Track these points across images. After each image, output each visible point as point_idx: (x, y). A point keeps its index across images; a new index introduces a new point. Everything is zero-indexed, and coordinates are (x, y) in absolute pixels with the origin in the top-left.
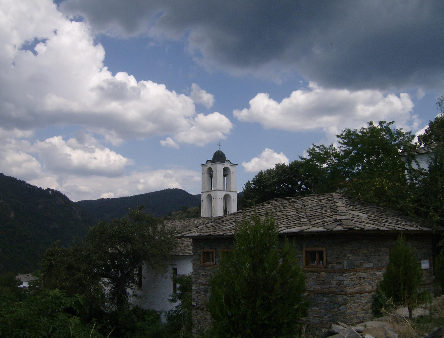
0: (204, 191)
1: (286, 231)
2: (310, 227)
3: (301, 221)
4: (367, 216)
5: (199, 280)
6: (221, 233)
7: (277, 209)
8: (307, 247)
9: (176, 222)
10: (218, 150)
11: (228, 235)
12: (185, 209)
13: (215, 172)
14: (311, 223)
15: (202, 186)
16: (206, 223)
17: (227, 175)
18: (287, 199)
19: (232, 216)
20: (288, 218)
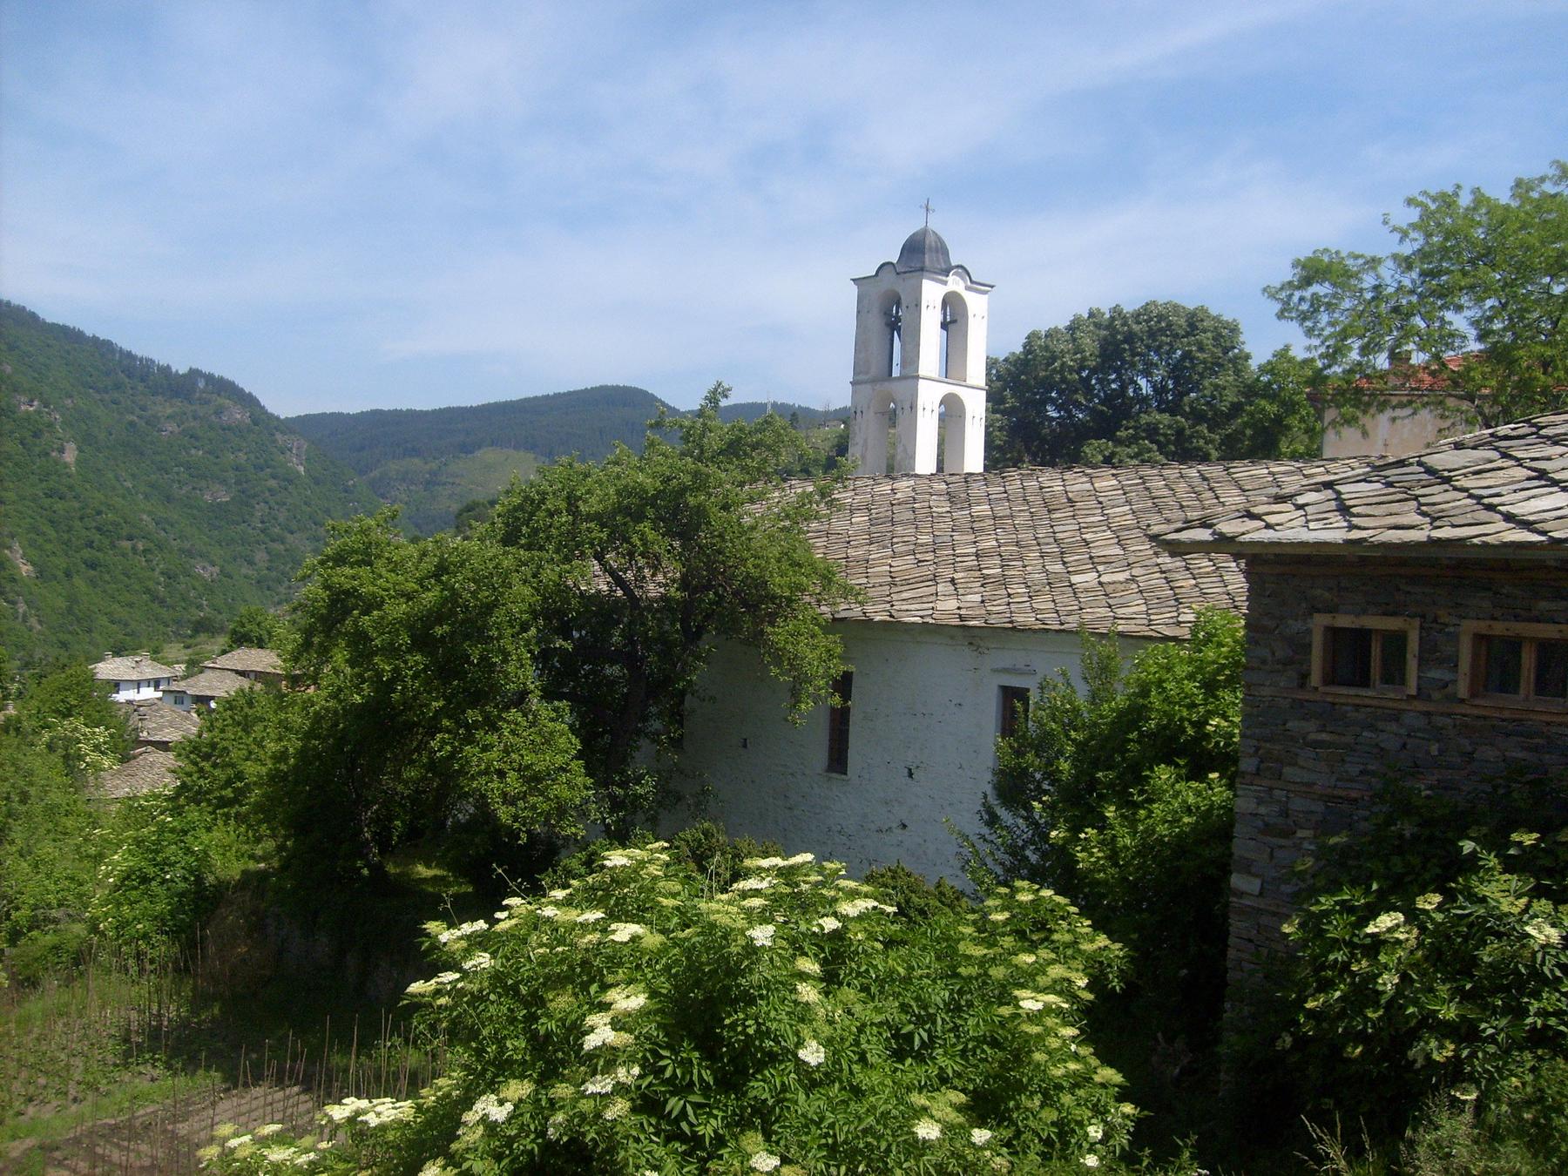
0: (862, 377)
17: (953, 321)
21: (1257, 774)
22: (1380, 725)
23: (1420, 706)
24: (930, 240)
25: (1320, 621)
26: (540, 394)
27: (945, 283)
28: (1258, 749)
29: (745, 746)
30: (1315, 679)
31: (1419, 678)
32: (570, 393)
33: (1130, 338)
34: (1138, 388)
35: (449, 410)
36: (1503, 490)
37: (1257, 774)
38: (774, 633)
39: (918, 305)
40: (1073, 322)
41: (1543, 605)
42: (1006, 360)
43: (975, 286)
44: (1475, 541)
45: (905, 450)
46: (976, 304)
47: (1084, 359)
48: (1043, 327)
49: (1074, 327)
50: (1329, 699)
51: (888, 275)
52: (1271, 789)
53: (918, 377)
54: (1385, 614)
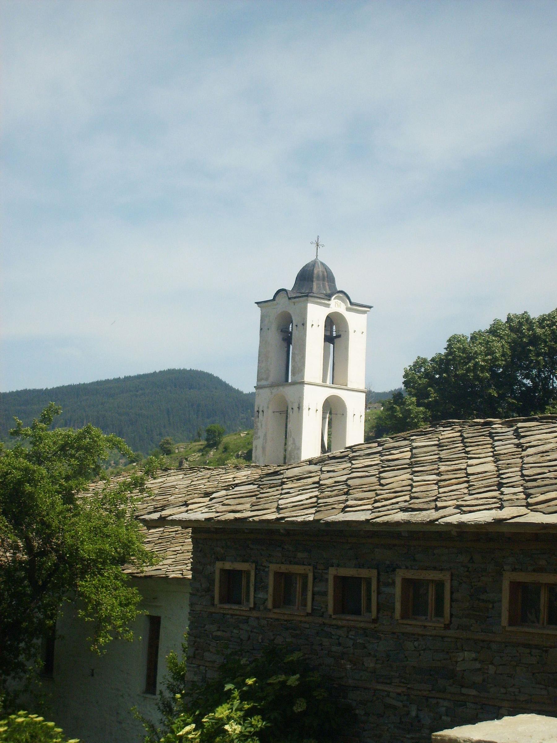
0: (263, 383)
1: (455, 519)
2: (524, 510)
3: (502, 493)
4: (522, 490)
5: (206, 654)
6: (273, 517)
7: (443, 454)
8: (514, 570)
9: (168, 475)
10: (313, 258)
11: (293, 522)
12: (212, 440)
13: (300, 325)
14: (529, 500)
15: (259, 367)
16: (237, 485)
17: (338, 336)
18: (478, 424)
19: (313, 468)
20: (467, 482)
21: (194, 657)
22: (241, 626)
23: (255, 614)
24: (318, 270)
25: (219, 565)
26: (111, 377)
27: (328, 306)
28: (195, 642)
29: (93, 675)
30: (216, 601)
31: (255, 597)
32: (139, 377)
33: (535, 340)
34: (525, 385)
35: (26, 392)
36: (291, 491)
37: (194, 657)
38: (82, 586)
39: (304, 324)
40: (493, 326)
41: (300, 555)
42: (433, 360)
43: (355, 306)
44: (251, 519)
45: (294, 443)
46: (356, 323)
47: (496, 359)
48: (466, 330)
49: (494, 331)
50: (222, 611)
51: (282, 300)
52: (199, 666)
53: (303, 383)
54: (243, 561)
